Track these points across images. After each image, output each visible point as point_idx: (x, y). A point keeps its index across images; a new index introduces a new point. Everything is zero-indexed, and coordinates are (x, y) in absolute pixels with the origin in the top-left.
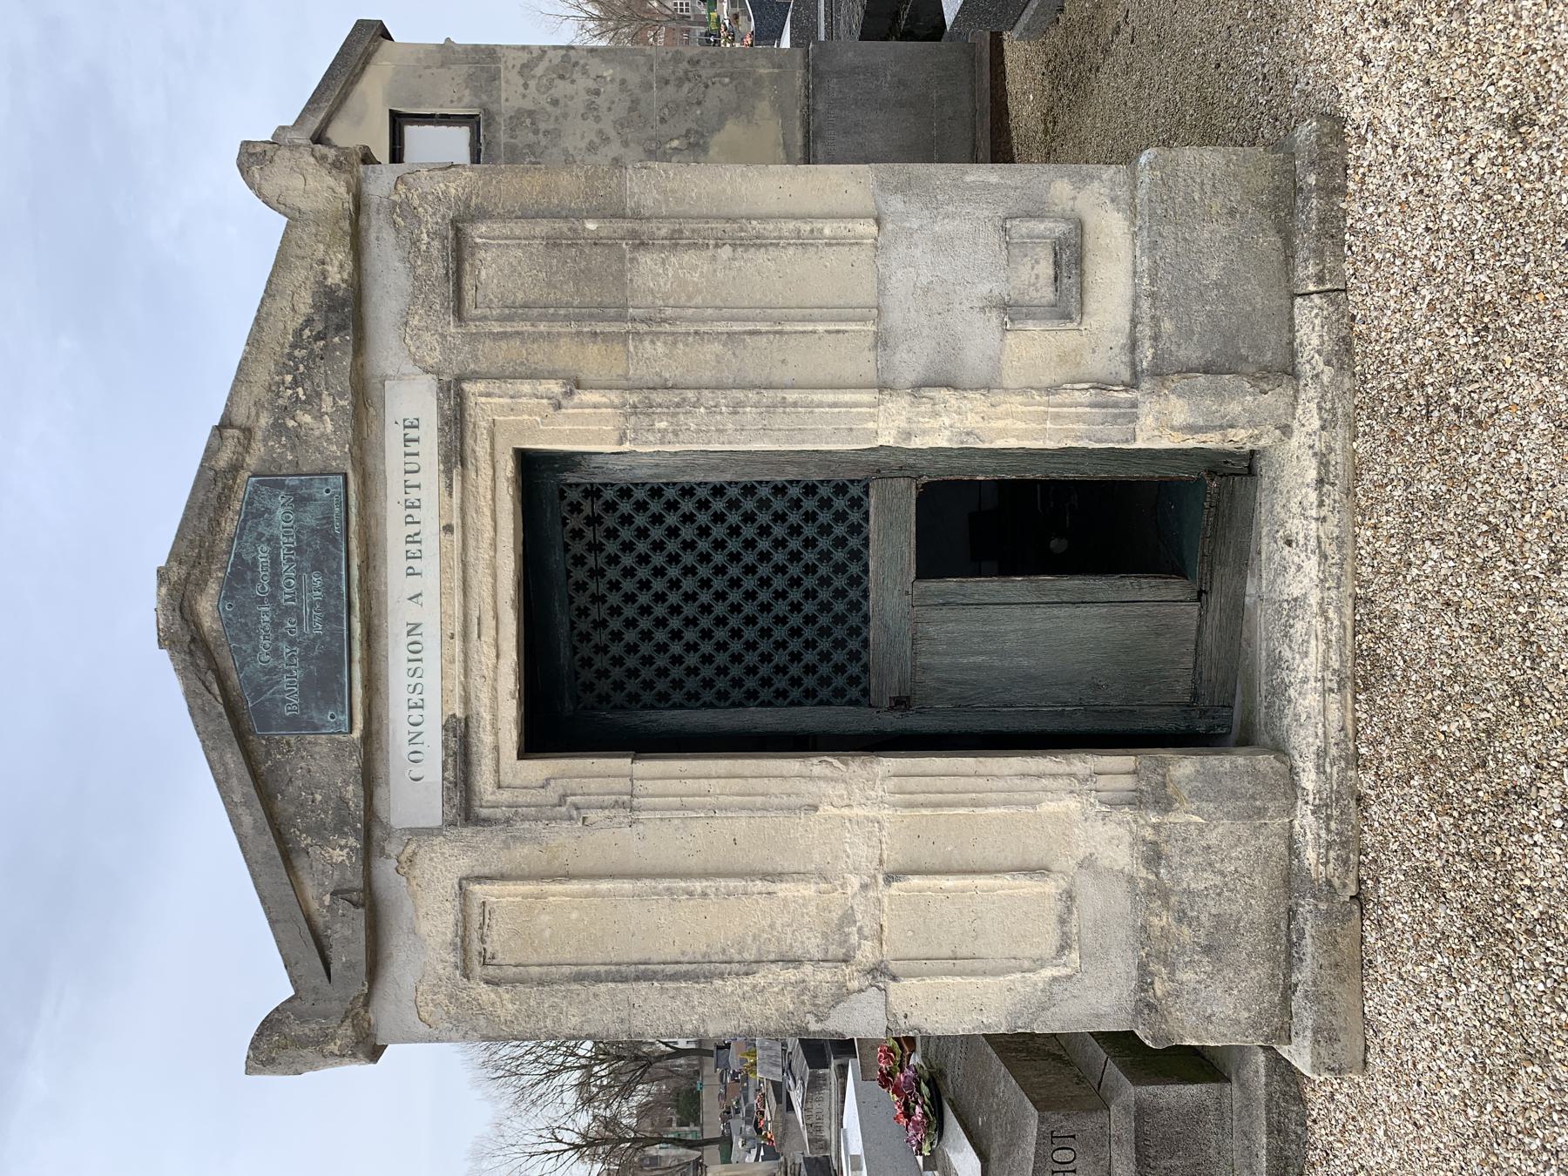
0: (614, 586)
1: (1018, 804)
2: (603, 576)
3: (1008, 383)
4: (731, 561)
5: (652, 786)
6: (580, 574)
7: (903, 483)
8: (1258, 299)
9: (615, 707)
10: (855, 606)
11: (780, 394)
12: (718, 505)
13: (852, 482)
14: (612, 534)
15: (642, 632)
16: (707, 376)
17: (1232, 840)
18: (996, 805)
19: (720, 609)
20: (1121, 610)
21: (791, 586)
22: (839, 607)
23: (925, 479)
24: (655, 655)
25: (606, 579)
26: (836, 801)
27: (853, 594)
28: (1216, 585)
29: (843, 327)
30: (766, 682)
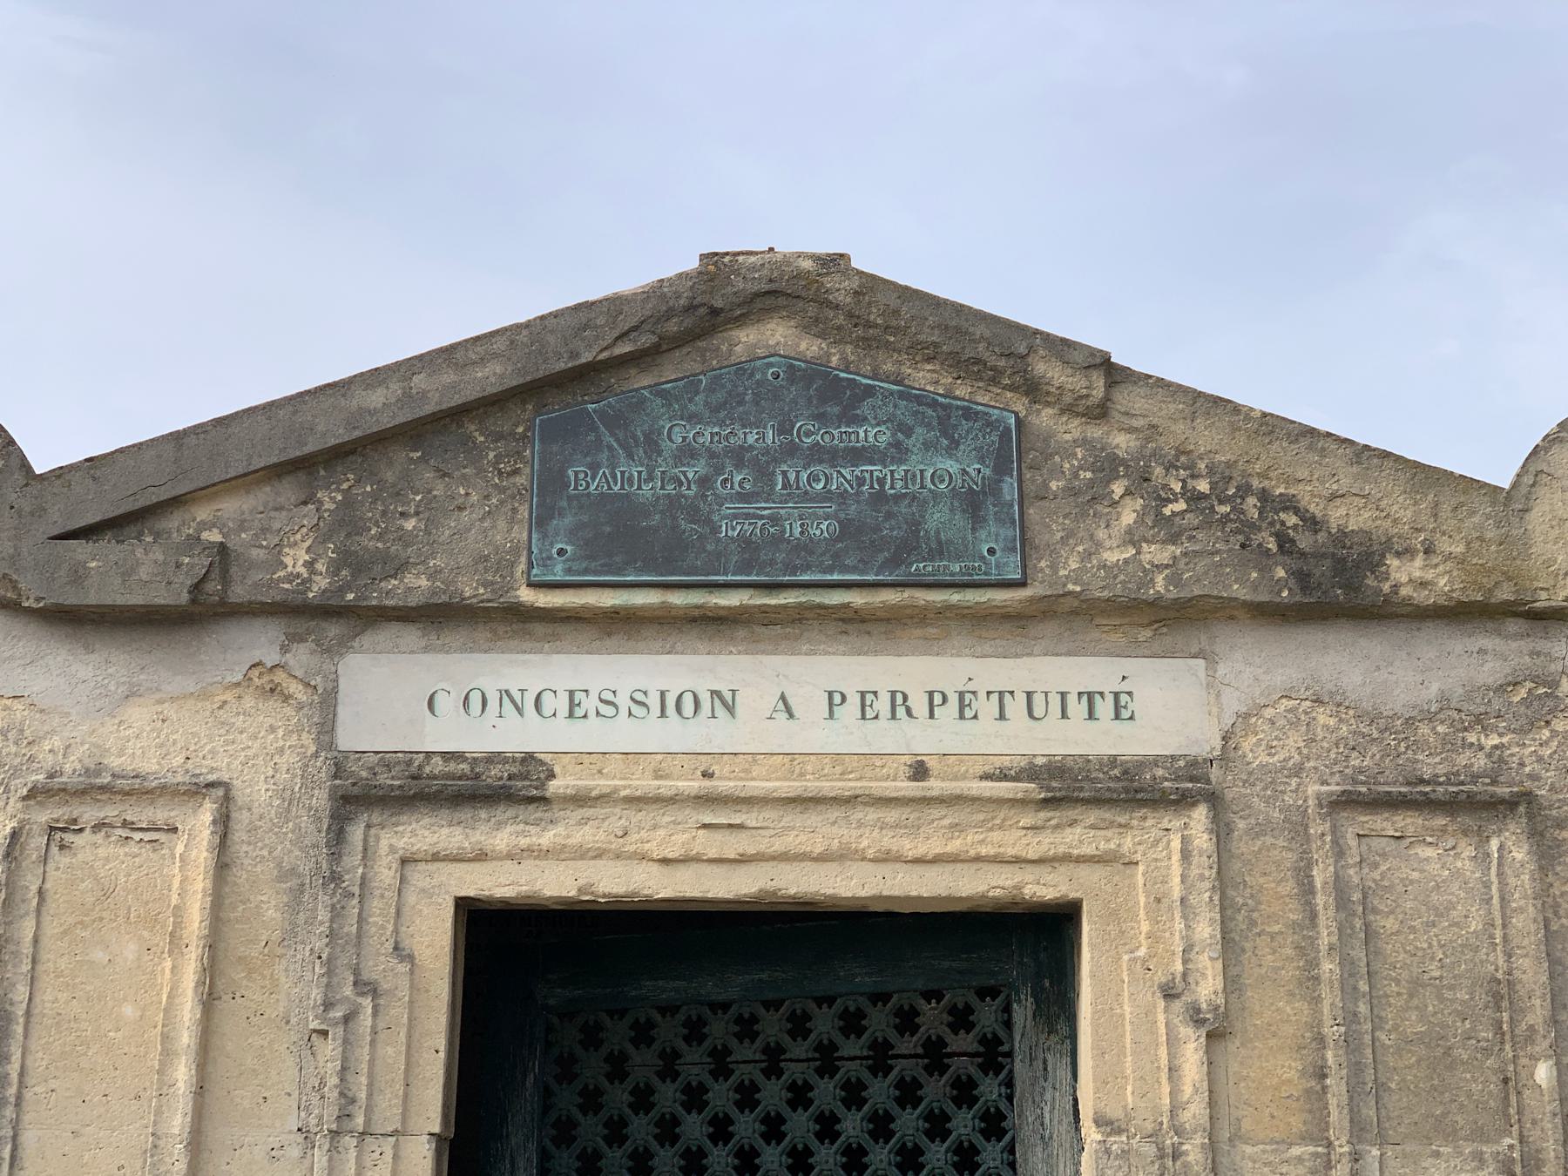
0: (800, 1096)
6: (824, 1024)
9: (547, 1093)
25: (814, 1079)
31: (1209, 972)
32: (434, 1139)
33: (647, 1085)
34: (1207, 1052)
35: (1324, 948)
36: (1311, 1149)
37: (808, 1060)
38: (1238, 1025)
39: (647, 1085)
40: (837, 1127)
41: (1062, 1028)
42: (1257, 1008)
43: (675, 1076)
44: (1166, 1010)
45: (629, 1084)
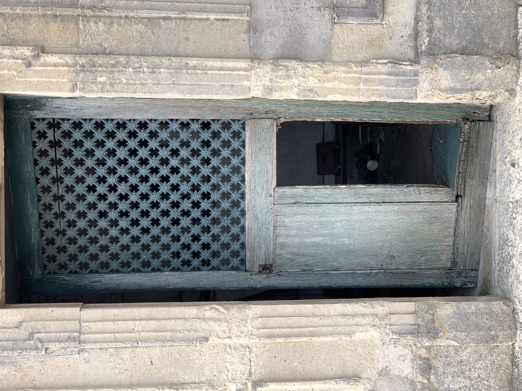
0: (70, 189)
1: (340, 334)
2: (62, 182)
3: (336, 58)
4: (152, 173)
5: (94, 326)
6: (45, 181)
7: (268, 122)
8: (496, 7)
9: (71, 272)
10: (236, 204)
11: (184, 60)
12: (143, 135)
13: (234, 121)
14: (68, 153)
15: (90, 221)
16: (134, 46)
17: (476, 357)
18: (325, 335)
19: (144, 205)
20: (407, 207)
21: (193, 190)
22: (225, 205)
23: (282, 120)
24: (99, 236)
25: (64, 184)
26: (221, 334)
27: (235, 196)
28: (468, 192)
29: (227, 17)
30: (177, 255)
31: (21, 51)
32: (82, 309)
33: (68, 240)
34: (49, 54)
35: (12, 12)
36: (80, 21)
37: (58, 186)
38: (39, 43)
39: (68, 240)
40: (80, 177)
41: (43, 101)
42: (34, 36)
43: (64, 231)
44: (35, 66)
45: (67, 246)
